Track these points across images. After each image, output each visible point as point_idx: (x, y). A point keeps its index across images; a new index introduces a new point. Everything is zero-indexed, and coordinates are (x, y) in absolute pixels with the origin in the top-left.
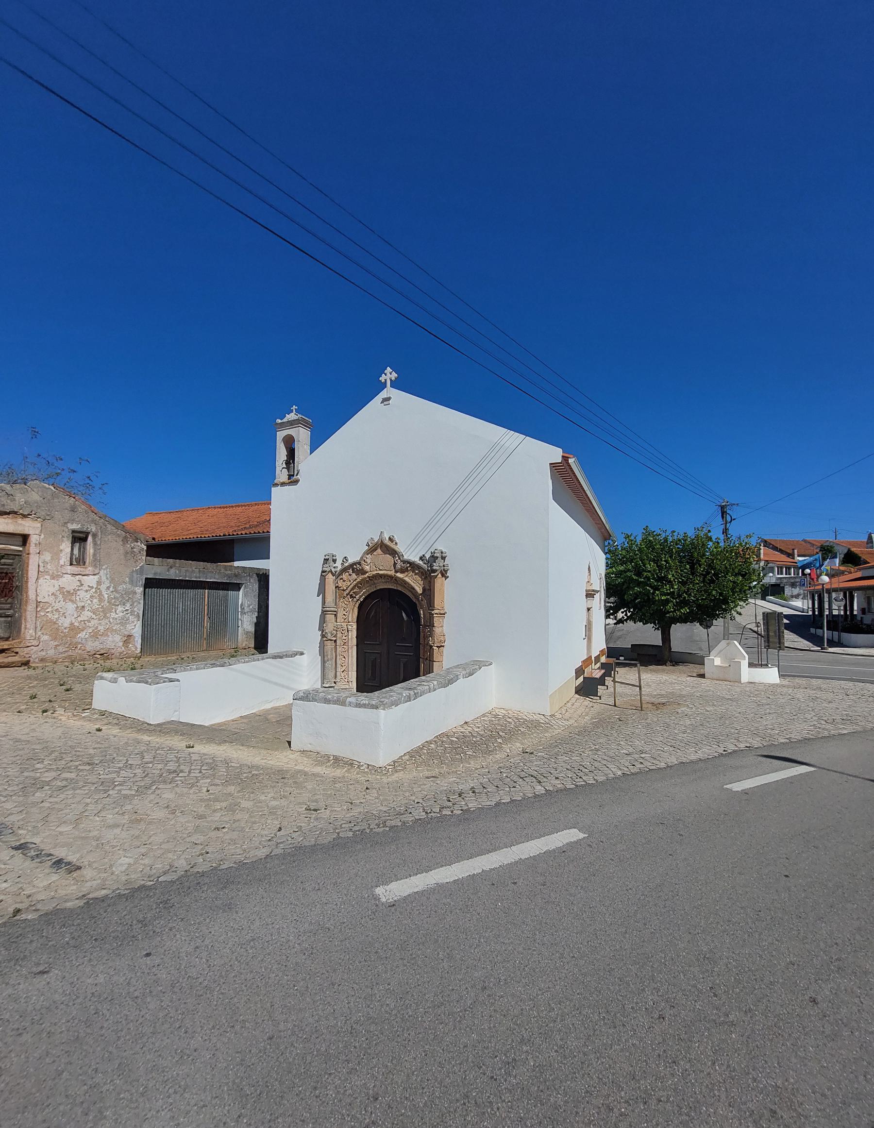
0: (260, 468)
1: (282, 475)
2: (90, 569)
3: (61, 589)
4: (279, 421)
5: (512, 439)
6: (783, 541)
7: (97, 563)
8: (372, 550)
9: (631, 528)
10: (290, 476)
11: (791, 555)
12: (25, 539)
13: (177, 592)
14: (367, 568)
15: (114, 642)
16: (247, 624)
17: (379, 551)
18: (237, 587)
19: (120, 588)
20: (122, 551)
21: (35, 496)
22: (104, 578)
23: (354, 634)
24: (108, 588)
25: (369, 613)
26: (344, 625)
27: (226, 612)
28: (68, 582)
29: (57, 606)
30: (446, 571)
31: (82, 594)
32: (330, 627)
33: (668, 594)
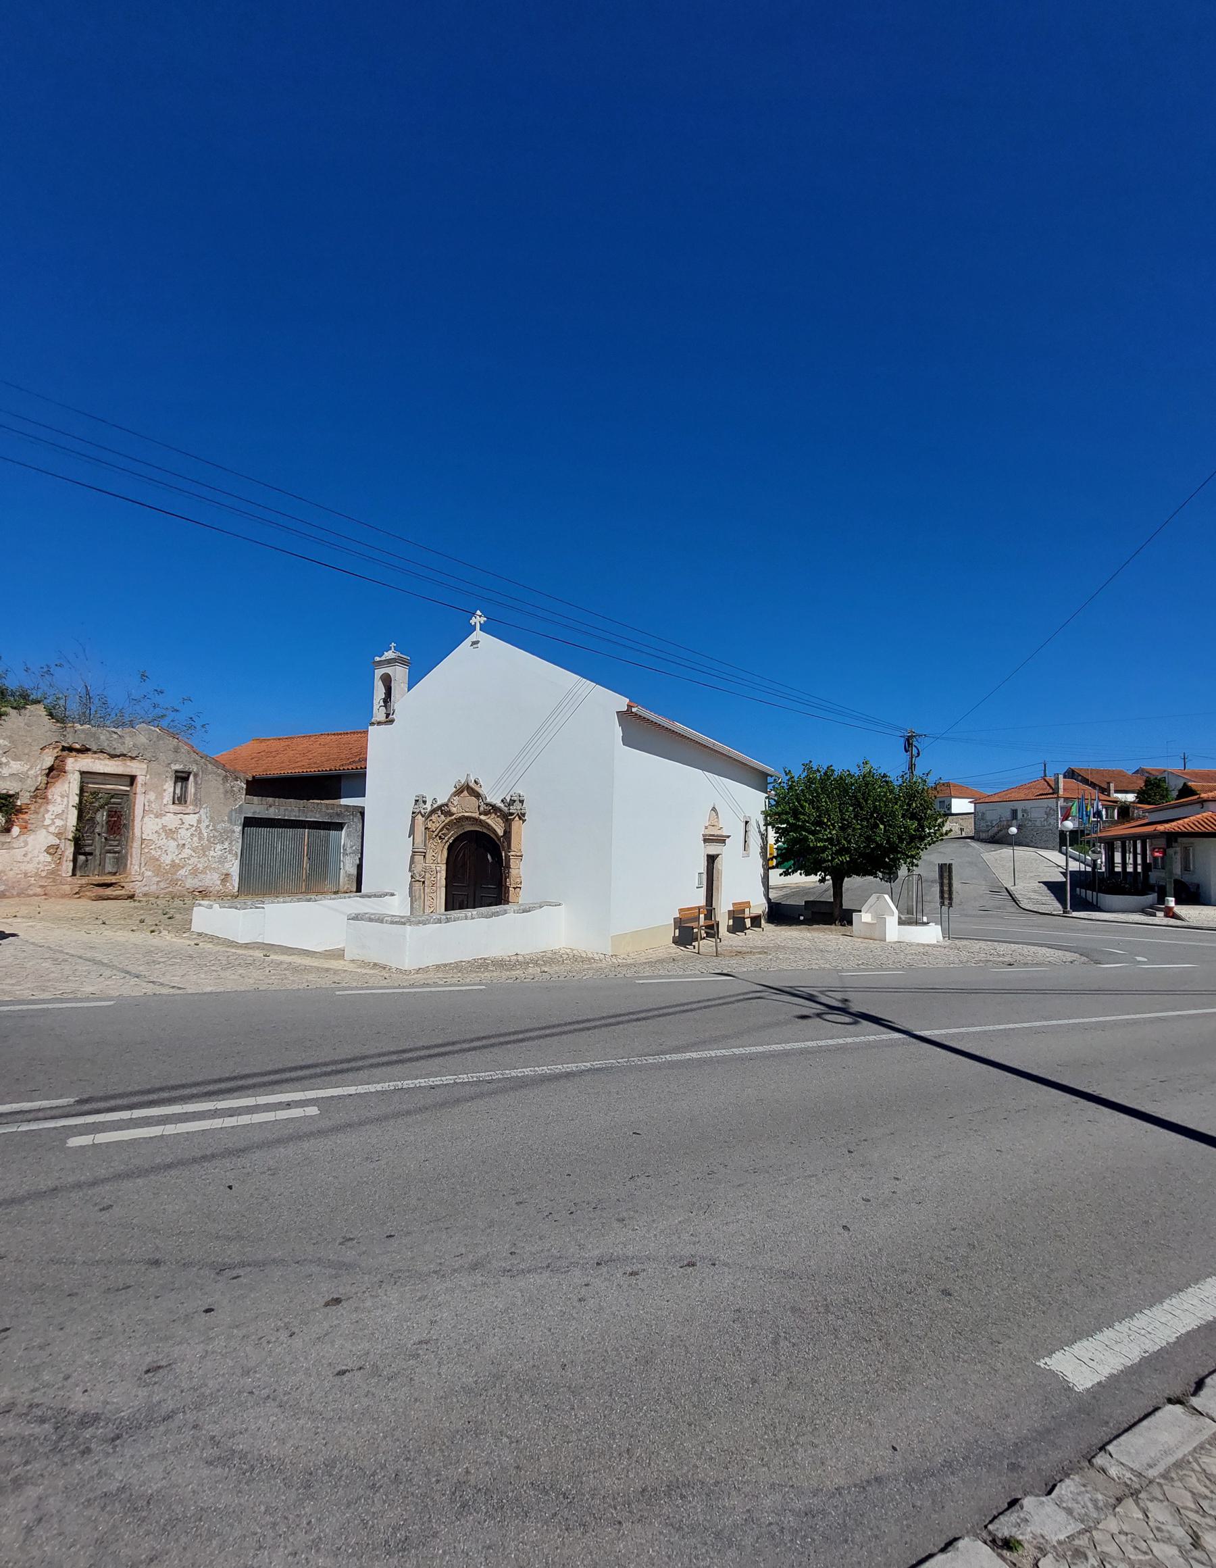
0: (360, 704)
1: (379, 714)
2: (191, 808)
3: (164, 827)
4: (377, 659)
5: (569, 679)
6: (1098, 771)
7: (198, 802)
8: (459, 792)
9: (790, 762)
10: (388, 715)
11: (1105, 790)
12: (132, 779)
13: (276, 831)
14: (454, 810)
15: (212, 880)
16: (349, 867)
17: (465, 792)
18: (339, 827)
19: (219, 827)
20: (221, 790)
21: (142, 739)
22: (204, 817)
23: (442, 880)
24: (208, 826)
25: (457, 856)
26: (433, 866)
27: (326, 853)
28: (171, 820)
29: (160, 843)
30: (524, 815)
31: (182, 832)
32: (418, 868)
33: (826, 841)
